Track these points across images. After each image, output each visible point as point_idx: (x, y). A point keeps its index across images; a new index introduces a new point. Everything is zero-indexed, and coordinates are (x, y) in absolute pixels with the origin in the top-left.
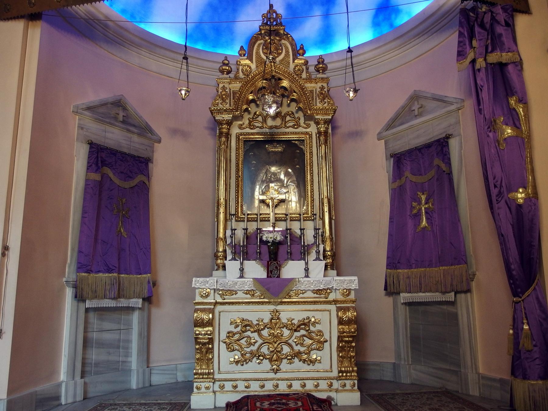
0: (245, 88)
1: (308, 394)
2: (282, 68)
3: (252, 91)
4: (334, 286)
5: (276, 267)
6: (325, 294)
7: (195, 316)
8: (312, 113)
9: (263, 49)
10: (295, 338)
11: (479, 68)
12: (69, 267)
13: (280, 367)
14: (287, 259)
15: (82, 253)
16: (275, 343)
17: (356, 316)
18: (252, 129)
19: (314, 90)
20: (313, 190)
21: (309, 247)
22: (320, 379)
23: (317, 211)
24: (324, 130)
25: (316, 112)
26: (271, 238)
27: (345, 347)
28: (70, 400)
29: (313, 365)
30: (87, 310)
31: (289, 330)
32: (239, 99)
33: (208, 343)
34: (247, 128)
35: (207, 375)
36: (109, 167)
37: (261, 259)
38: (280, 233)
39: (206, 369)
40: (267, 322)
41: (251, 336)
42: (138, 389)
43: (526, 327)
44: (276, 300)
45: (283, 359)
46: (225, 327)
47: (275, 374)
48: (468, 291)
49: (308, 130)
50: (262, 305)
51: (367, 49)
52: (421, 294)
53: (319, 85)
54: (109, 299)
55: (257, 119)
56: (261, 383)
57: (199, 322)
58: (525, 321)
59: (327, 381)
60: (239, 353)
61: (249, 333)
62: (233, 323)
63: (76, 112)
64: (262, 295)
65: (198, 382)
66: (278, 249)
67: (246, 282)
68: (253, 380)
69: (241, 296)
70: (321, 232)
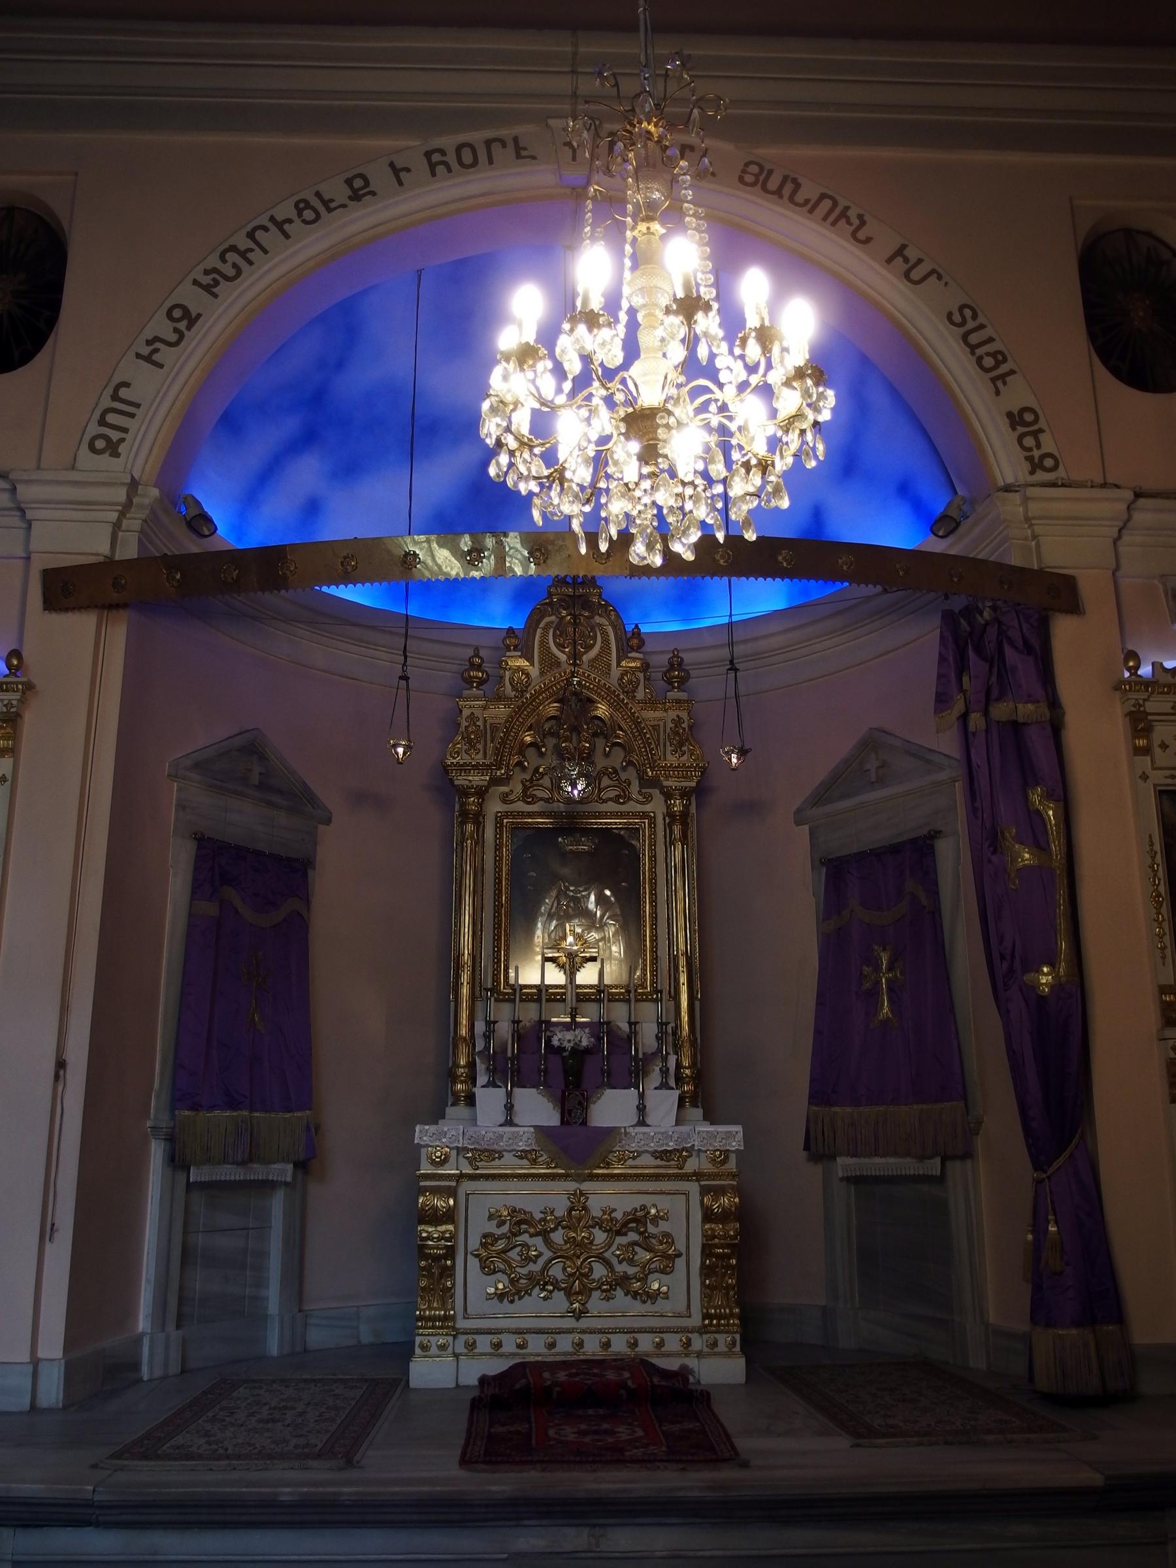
0: (517, 720)
1: (642, 1360)
2: (595, 678)
3: (531, 724)
4: (696, 1143)
5: (580, 1103)
7: (421, 1201)
8: (656, 774)
10: (618, 1249)
11: (974, 730)
13: (587, 1305)
14: (602, 1086)
16: (578, 1257)
17: (738, 1204)
18: (529, 803)
19: (662, 724)
20: (656, 937)
21: (649, 1058)
22: (666, 1332)
23: (663, 984)
24: (680, 811)
25: (665, 774)
26: (569, 1041)
27: (717, 1267)
28: (158, 1373)
29: (653, 1304)
31: (604, 1231)
32: (503, 742)
33: (445, 1257)
34: (519, 800)
35: (442, 1322)
37: (547, 1086)
38: (587, 1030)
39: (439, 1309)
40: (562, 1214)
41: (530, 1244)
43: (1052, 1228)
44: (581, 1171)
45: (592, 1289)
46: (479, 1225)
47: (578, 1320)
48: (967, 1155)
50: (552, 1180)
52: (878, 1160)
53: (672, 714)
54: (233, 1163)
56: (549, 1339)
57: (428, 1213)
58: (1051, 1217)
59: (678, 1336)
60: (505, 1278)
61: (525, 1237)
62: (492, 1217)
63: (173, 777)
64: (553, 1160)
65: (425, 1335)
67: (521, 1133)
68: (533, 1333)
69: (509, 1164)
70: (672, 1028)
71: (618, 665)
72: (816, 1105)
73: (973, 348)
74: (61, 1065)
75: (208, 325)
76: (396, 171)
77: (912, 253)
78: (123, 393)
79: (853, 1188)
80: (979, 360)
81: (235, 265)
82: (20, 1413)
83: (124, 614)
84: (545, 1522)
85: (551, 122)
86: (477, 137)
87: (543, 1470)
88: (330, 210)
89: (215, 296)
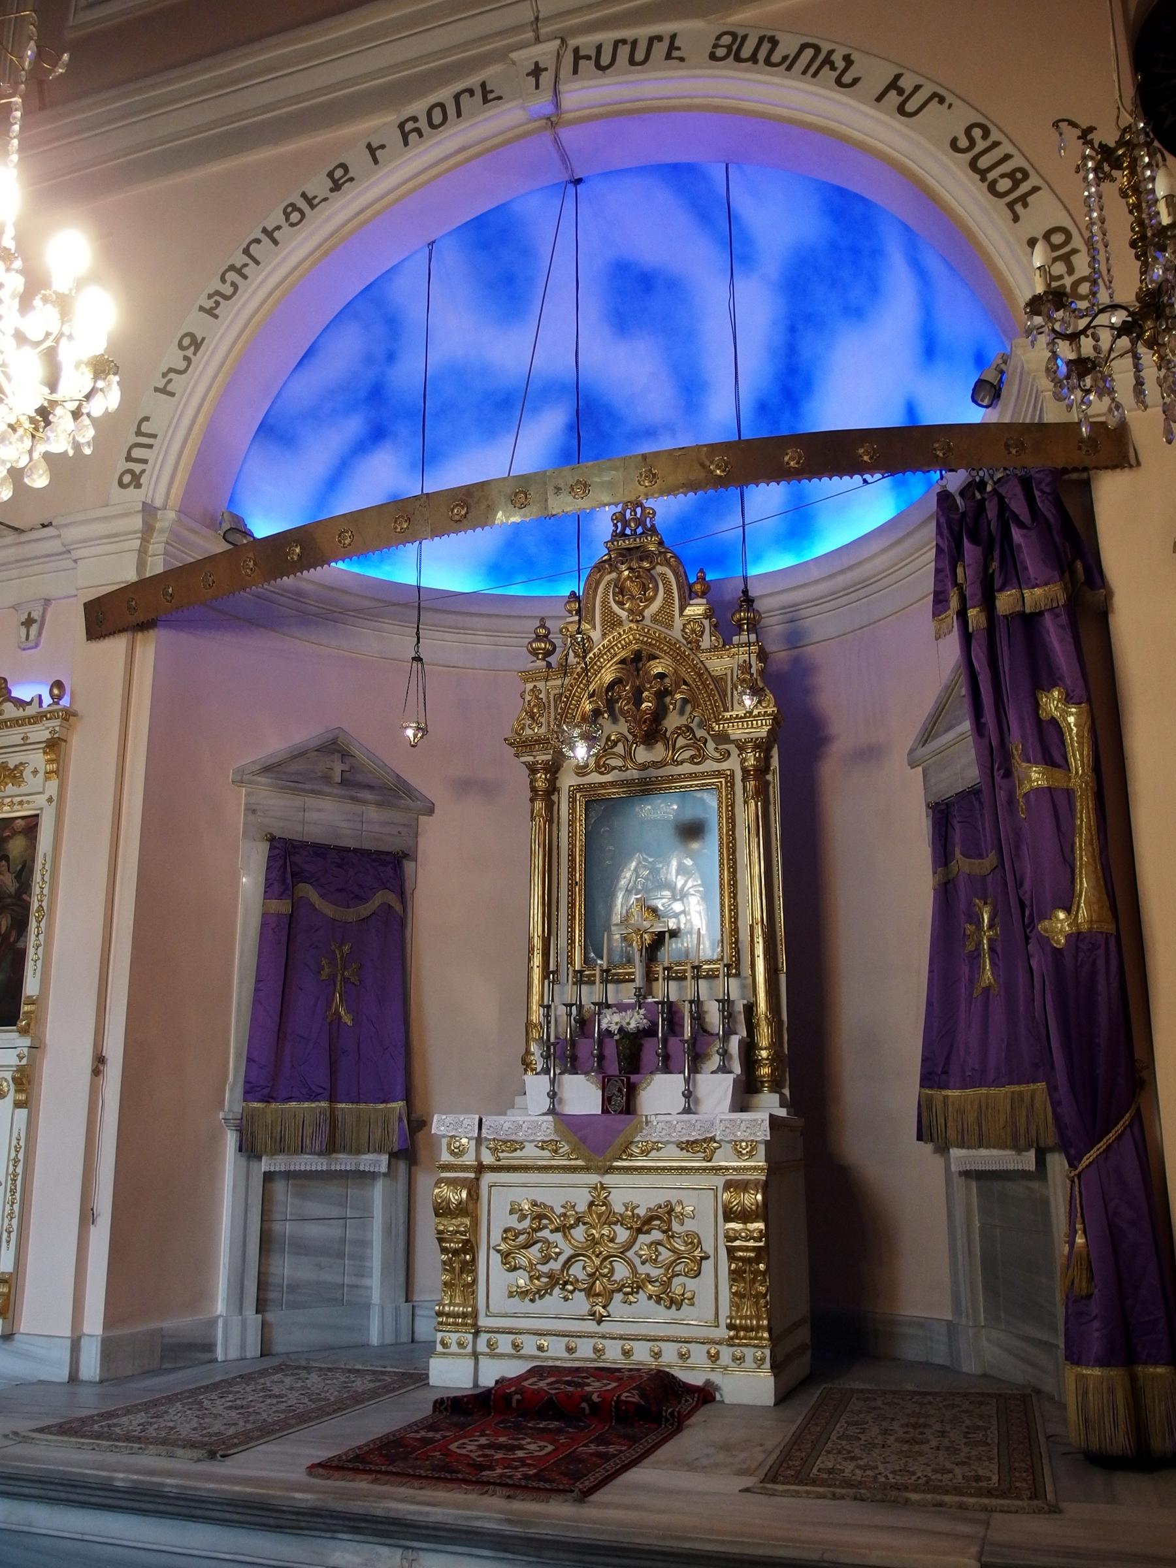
3: (594, 690)
6: (705, 1152)
9: (614, 595)
12: (231, 1090)
13: (608, 1308)
15: (254, 1061)
18: (602, 773)
19: (729, 672)
28: (233, 1354)
30: (268, 1177)
31: (627, 1229)
36: (311, 884)
41: (551, 1241)
42: (382, 1346)
49: (724, 766)
51: (875, 546)
52: (983, 1152)
54: (311, 1153)
55: (615, 750)
61: (545, 1233)
63: (238, 782)
66: (639, 1048)
71: (681, 614)
72: (931, 1087)
73: (983, 174)
74: (100, 1060)
75: (212, 347)
76: (372, 150)
77: (907, 83)
78: (145, 427)
79: (974, 1184)
80: (992, 188)
81: (233, 284)
82: (61, 1384)
83: (152, 634)
84: (359, 1538)
85: (513, 55)
86: (444, 94)
87: (373, 1482)
88: (312, 207)
89: (216, 317)
